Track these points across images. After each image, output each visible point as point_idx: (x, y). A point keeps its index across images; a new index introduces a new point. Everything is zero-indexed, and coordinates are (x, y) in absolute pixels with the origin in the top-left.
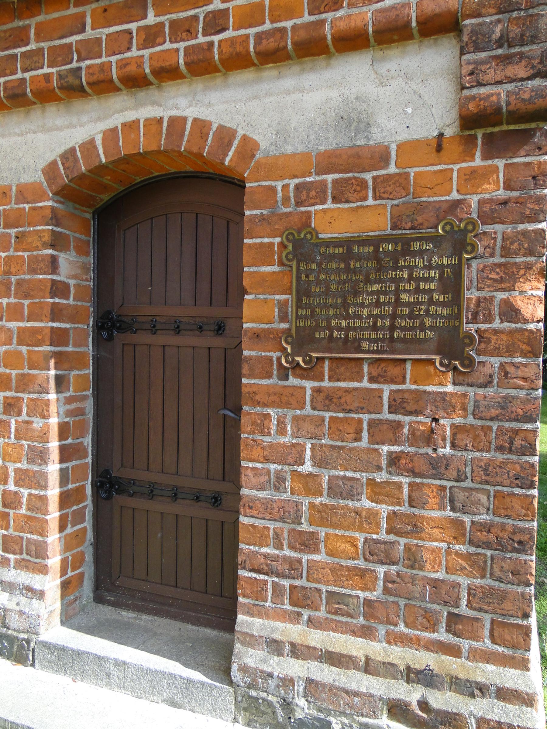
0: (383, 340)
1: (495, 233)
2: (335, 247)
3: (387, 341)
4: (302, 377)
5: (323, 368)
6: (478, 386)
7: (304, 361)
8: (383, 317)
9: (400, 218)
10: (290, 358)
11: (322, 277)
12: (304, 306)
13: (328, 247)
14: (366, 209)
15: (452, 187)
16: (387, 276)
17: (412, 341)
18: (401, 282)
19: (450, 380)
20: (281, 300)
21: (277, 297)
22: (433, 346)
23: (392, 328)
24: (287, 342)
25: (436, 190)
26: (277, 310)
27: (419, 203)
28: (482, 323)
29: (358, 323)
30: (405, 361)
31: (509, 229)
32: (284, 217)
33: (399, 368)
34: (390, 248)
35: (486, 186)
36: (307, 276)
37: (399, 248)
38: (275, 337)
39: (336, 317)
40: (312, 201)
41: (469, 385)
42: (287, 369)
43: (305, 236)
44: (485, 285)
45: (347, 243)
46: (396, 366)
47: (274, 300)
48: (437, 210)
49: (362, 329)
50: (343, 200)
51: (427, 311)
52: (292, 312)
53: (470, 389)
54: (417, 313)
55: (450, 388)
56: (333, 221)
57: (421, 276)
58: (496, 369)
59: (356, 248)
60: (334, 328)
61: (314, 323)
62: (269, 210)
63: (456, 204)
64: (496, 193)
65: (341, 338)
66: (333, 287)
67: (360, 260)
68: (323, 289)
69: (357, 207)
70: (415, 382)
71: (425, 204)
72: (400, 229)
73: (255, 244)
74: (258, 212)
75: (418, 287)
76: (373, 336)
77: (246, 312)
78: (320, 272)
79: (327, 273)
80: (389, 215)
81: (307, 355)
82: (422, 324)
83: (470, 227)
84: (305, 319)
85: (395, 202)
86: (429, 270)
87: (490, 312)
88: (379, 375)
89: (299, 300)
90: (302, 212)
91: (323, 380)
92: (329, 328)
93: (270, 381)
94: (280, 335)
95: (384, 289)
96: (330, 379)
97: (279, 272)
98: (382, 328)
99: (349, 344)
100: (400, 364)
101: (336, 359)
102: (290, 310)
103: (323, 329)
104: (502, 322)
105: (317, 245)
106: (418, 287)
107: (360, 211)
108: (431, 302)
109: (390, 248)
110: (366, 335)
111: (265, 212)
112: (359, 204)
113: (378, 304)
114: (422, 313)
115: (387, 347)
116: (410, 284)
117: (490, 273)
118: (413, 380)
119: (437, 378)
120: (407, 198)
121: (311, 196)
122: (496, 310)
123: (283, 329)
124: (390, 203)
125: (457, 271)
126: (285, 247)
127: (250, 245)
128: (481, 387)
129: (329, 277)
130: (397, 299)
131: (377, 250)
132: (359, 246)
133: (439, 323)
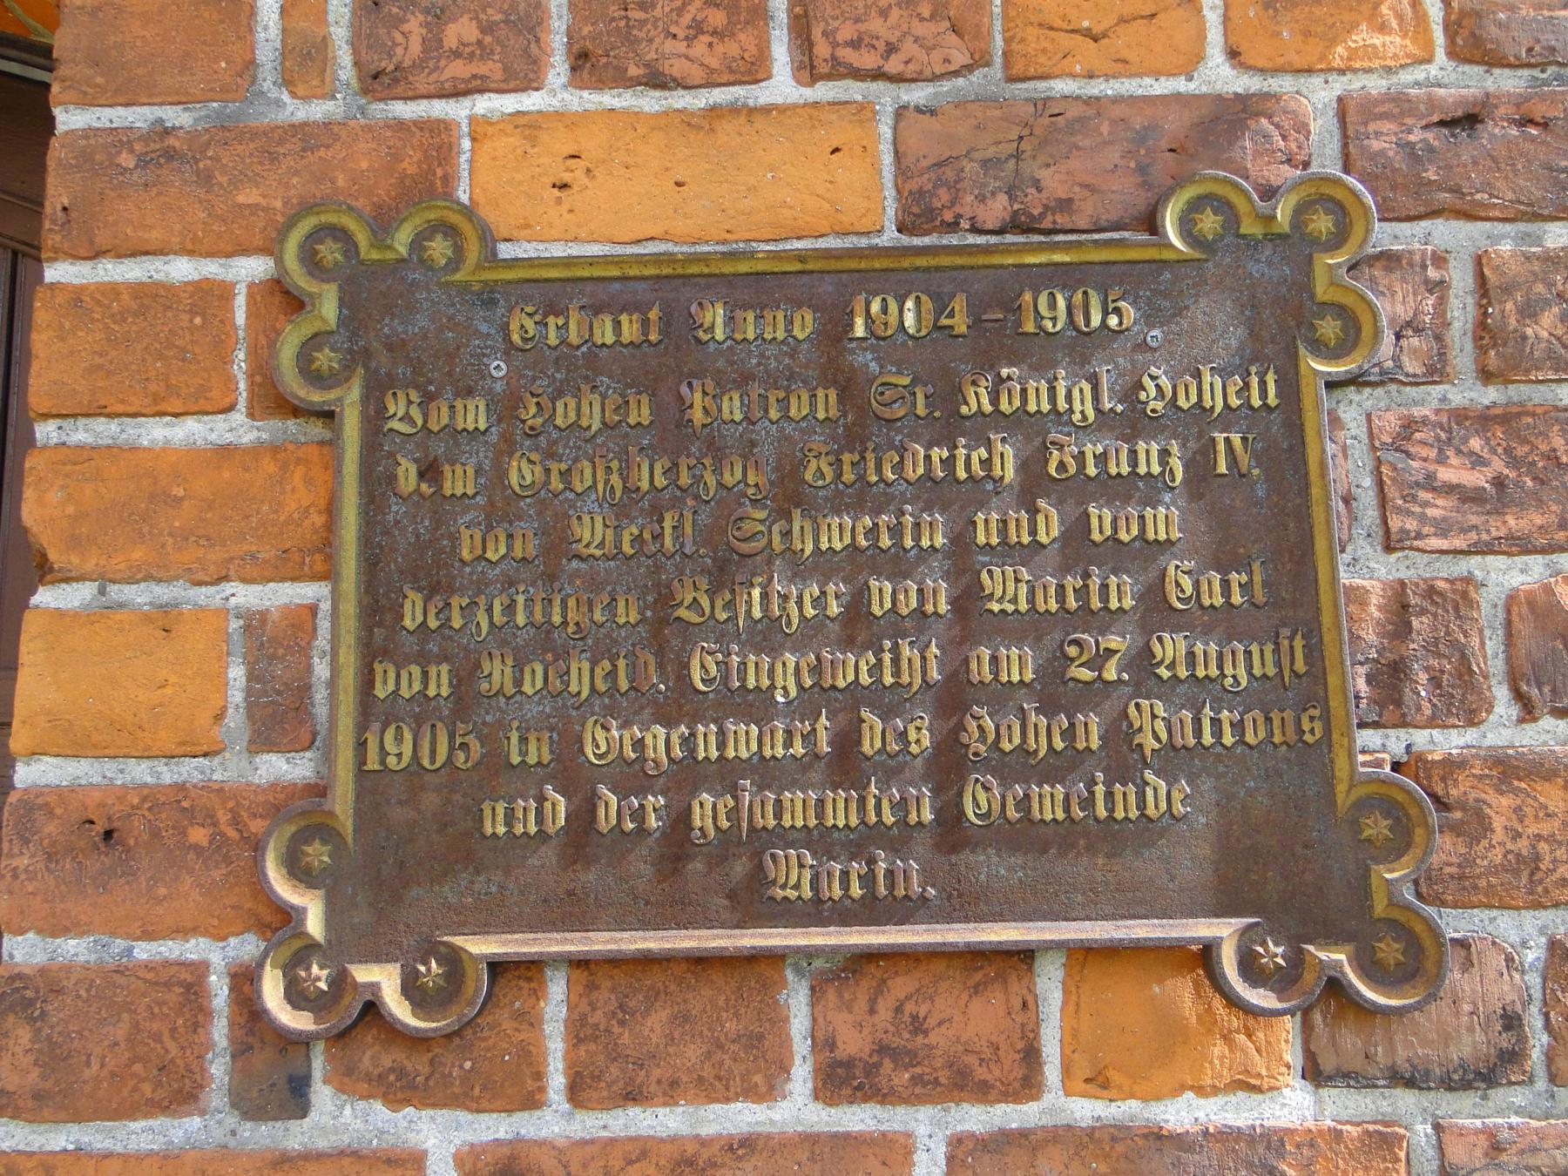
0: (899, 839)
1: (1440, 260)
2: (597, 310)
3: (922, 844)
4: (400, 1090)
5: (531, 1020)
6: (1449, 1085)
7: (411, 988)
8: (890, 702)
9: (949, 174)
10: (320, 975)
11: (522, 473)
12: (410, 644)
13: (553, 309)
14: (759, 122)
15: (1201, 36)
16: (899, 467)
17: (1068, 836)
18: (982, 504)
19: (1292, 1055)
20: (263, 615)
21: (245, 595)
22: (1191, 860)
23: (949, 765)
24: (298, 871)
25: (1121, 42)
26: (237, 673)
27: (1042, 104)
28: (1431, 723)
29: (744, 741)
30: (1024, 956)
31: (1505, 242)
32: (294, 145)
33: (996, 997)
34: (909, 320)
35: (1363, 36)
36: (430, 471)
37: (960, 323)
38: (219, 844)
39: (611, 705)
40: (458, 70)
41: (1410, 1080)
42: (302, 1042)
43: (417, 244)
44: (1423, 519)
45: (667, 291)
46: (976, 990)
47: (223, 612)
48: (1141, 138)
49: (766, 772)
50: (633, 71)
51: (1142, 661)
52: (332, 684)
53: (1405, 1101)
54: (1086, 674)
55: (1293, 1106)
56: (577, 176)
57: (1092, 471)
58: (1534, 980)
59: (716, 316)
60: (596, 774)
61: (476, 749)
62: (200, 111)
63: (1229, 118)
64: (1419, 74)
65: (642, 831)
66: (591, 532)
67: (743, 380)
68: (526, 546)
69: (714, 111)
70: (1099, 1084)
71: (1074, 111)
72: (953, 227)
73: (112, 290)
74: (138, 117)
75: (1077, 530)
76: (841, 814)
77: (35, 687)
78: (508, 447)
79: (551, 455)
80: (887, 159)
81: (430, 949)
82: (1120, 734)
83: (1322, 224)
84: (418, 722)
85: (917, 95)
86: (1131, 439)
87: (1464, 658)
88: (882, 1049)
89: (378, 610)
90: (400, 125)
91: (533, 1101)
92: (569, 771)
93: (182, 1130)
94: (257, 826)
95: (885, 542)
96: (577, 1093)
97: (257, 450)
98: (891, 768)
99: (697, 866)
100: (1002, 977)
101: (615, 962)
102: (321, 670)
103: (529, 779)
104: (1528, 711)
105: (488, 297)
106: (1077, 530)
107: (728, 130)
108: (1156, 610)
109: (909, 320)
110: (798, 807)
111: (176, 116)
112: (719, 96)
113: (858, 626)
114: (1111, 674)
115: (928, 878)
116: (1034, 511)
117: (1442, 460)
118: (1083, 1070)
119: (1218, 1049)
120: (977, 77)
121: (450, 42)
122: (1491, 654)
123: (274, 786)
124: (886, 97)
125: (1285, 443)
126: (295, 303)
127: (77, 297)
128: (1466, 1086)
129: (565, 475)
130: (968, 600)
131: (835, 330)
132: (732, 308)
133: (1219, 727)
